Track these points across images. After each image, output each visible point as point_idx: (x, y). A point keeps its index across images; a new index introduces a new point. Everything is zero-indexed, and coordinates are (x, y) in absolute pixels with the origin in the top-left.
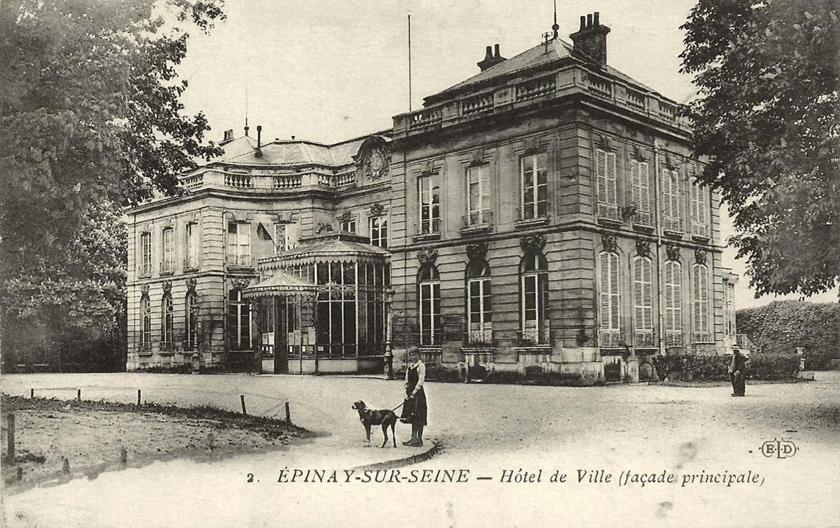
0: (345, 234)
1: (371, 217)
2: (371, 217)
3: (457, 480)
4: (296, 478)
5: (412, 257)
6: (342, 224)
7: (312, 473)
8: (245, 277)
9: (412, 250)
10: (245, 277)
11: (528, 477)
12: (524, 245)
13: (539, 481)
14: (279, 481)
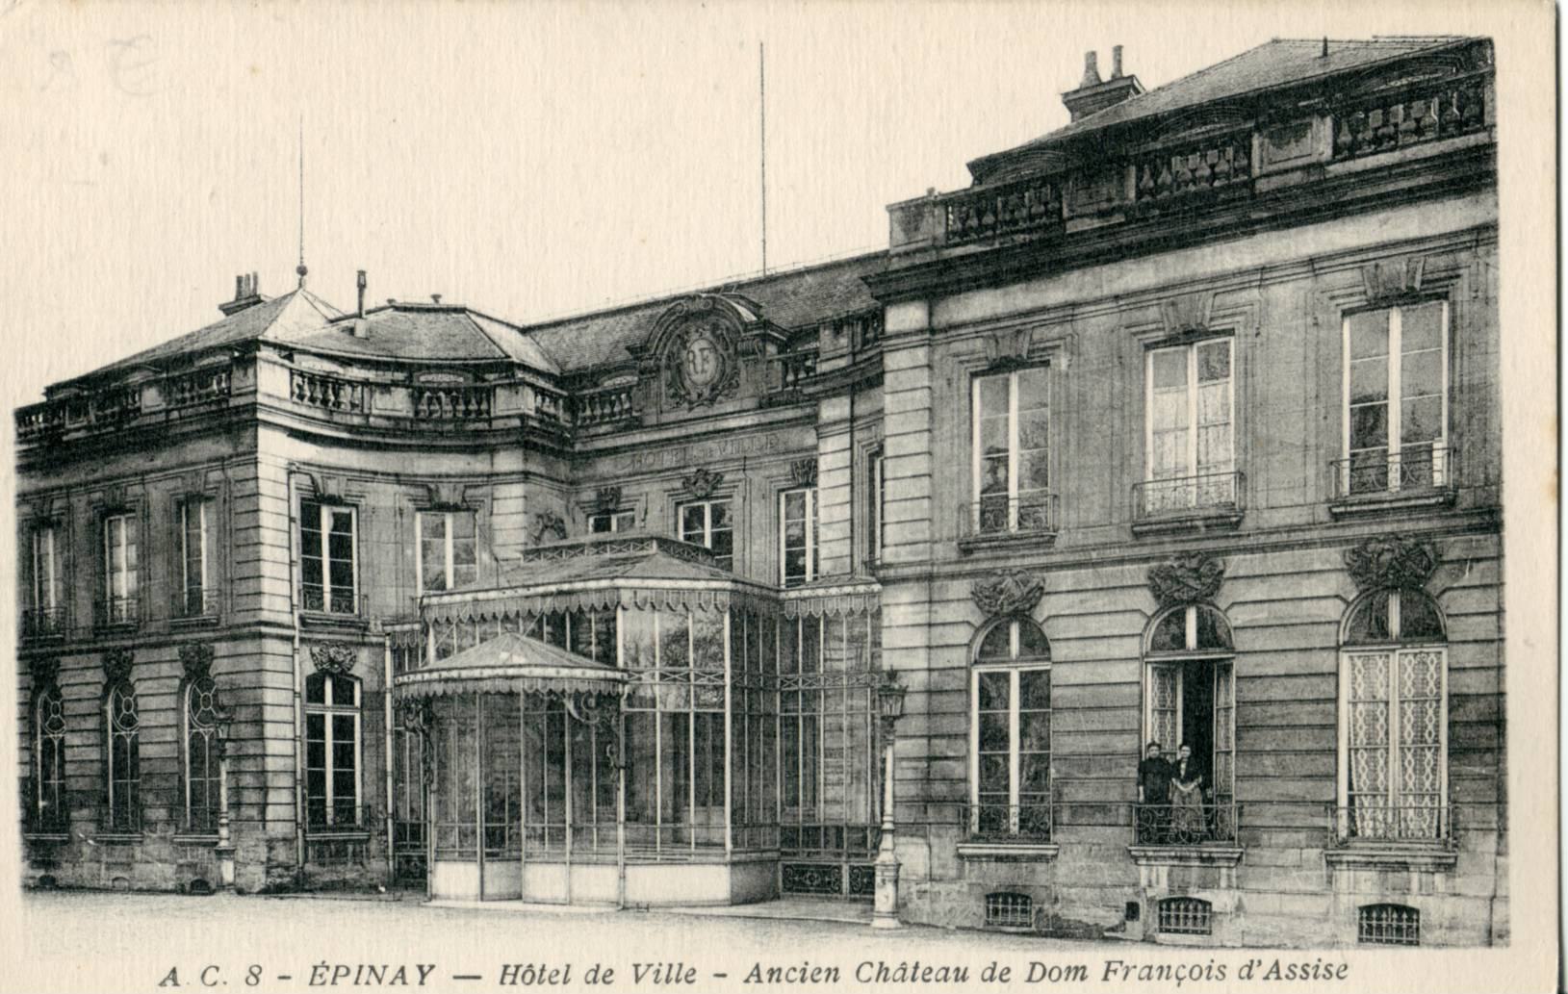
0: (671, 536)
1: (783, 490)
2: (783, 490)
3: (1026, 977)
4: (338, 980)
5: (951, 597)
6: (681, 510)
7: (366, 971)
8: (346, 645)
9: (953, 576)
10: (346, 645)
11: (546, 975)
12: (1361, 565)
13: (565, 982)
14: (311, 984)
